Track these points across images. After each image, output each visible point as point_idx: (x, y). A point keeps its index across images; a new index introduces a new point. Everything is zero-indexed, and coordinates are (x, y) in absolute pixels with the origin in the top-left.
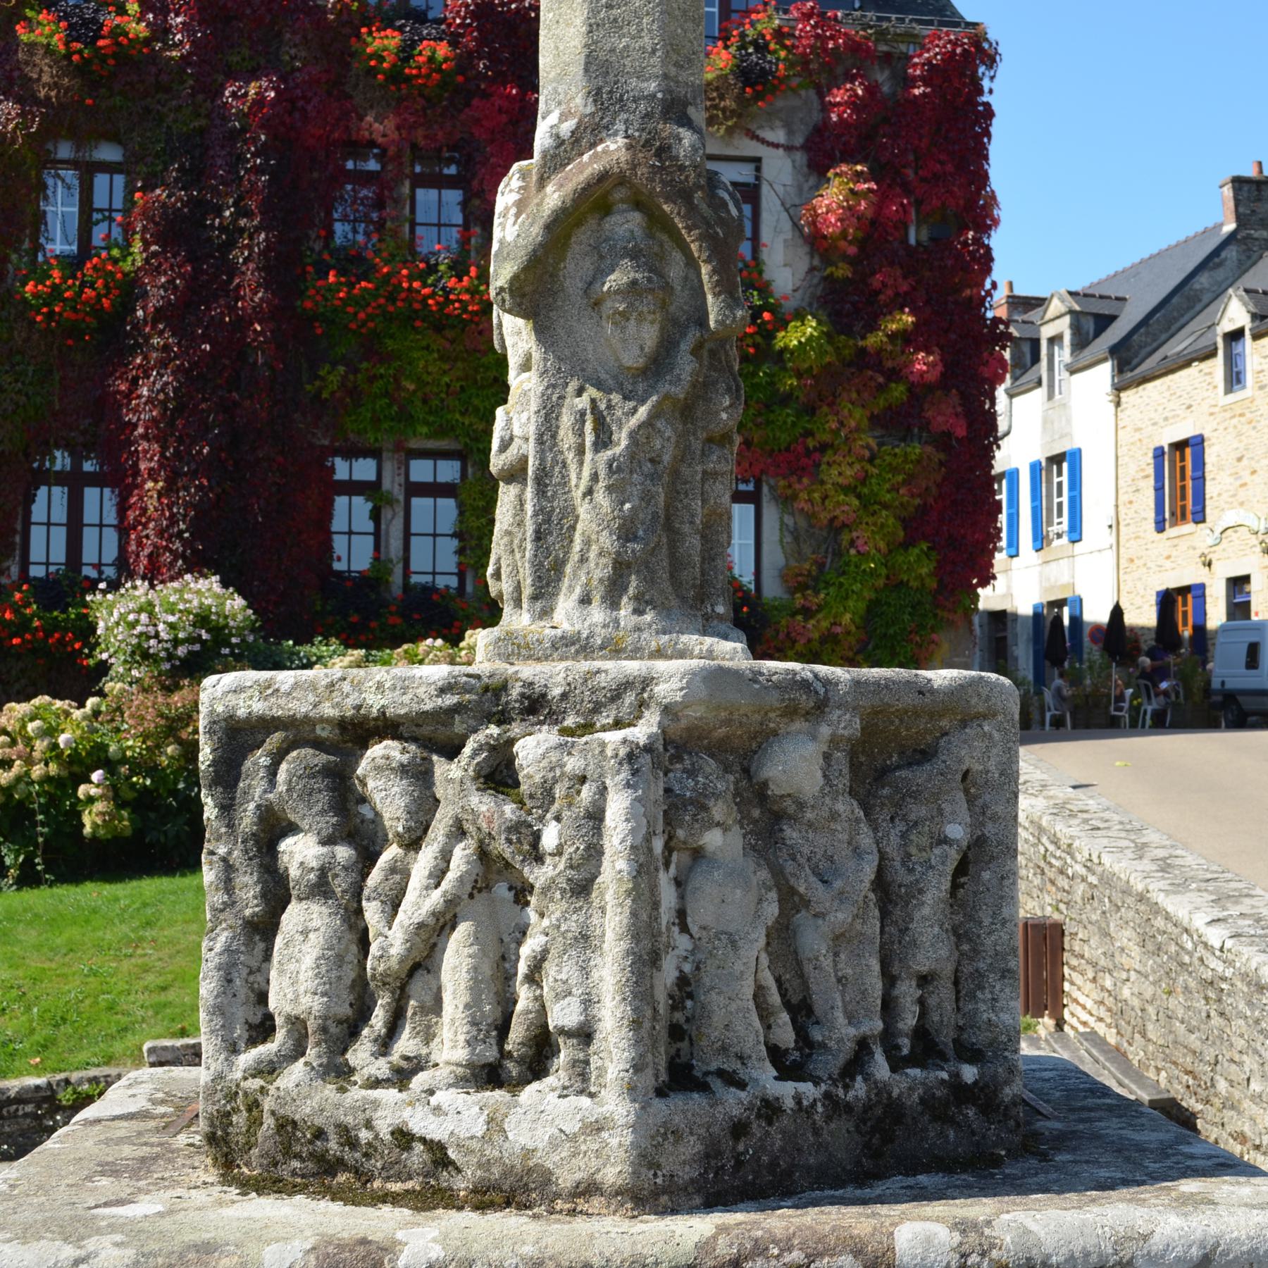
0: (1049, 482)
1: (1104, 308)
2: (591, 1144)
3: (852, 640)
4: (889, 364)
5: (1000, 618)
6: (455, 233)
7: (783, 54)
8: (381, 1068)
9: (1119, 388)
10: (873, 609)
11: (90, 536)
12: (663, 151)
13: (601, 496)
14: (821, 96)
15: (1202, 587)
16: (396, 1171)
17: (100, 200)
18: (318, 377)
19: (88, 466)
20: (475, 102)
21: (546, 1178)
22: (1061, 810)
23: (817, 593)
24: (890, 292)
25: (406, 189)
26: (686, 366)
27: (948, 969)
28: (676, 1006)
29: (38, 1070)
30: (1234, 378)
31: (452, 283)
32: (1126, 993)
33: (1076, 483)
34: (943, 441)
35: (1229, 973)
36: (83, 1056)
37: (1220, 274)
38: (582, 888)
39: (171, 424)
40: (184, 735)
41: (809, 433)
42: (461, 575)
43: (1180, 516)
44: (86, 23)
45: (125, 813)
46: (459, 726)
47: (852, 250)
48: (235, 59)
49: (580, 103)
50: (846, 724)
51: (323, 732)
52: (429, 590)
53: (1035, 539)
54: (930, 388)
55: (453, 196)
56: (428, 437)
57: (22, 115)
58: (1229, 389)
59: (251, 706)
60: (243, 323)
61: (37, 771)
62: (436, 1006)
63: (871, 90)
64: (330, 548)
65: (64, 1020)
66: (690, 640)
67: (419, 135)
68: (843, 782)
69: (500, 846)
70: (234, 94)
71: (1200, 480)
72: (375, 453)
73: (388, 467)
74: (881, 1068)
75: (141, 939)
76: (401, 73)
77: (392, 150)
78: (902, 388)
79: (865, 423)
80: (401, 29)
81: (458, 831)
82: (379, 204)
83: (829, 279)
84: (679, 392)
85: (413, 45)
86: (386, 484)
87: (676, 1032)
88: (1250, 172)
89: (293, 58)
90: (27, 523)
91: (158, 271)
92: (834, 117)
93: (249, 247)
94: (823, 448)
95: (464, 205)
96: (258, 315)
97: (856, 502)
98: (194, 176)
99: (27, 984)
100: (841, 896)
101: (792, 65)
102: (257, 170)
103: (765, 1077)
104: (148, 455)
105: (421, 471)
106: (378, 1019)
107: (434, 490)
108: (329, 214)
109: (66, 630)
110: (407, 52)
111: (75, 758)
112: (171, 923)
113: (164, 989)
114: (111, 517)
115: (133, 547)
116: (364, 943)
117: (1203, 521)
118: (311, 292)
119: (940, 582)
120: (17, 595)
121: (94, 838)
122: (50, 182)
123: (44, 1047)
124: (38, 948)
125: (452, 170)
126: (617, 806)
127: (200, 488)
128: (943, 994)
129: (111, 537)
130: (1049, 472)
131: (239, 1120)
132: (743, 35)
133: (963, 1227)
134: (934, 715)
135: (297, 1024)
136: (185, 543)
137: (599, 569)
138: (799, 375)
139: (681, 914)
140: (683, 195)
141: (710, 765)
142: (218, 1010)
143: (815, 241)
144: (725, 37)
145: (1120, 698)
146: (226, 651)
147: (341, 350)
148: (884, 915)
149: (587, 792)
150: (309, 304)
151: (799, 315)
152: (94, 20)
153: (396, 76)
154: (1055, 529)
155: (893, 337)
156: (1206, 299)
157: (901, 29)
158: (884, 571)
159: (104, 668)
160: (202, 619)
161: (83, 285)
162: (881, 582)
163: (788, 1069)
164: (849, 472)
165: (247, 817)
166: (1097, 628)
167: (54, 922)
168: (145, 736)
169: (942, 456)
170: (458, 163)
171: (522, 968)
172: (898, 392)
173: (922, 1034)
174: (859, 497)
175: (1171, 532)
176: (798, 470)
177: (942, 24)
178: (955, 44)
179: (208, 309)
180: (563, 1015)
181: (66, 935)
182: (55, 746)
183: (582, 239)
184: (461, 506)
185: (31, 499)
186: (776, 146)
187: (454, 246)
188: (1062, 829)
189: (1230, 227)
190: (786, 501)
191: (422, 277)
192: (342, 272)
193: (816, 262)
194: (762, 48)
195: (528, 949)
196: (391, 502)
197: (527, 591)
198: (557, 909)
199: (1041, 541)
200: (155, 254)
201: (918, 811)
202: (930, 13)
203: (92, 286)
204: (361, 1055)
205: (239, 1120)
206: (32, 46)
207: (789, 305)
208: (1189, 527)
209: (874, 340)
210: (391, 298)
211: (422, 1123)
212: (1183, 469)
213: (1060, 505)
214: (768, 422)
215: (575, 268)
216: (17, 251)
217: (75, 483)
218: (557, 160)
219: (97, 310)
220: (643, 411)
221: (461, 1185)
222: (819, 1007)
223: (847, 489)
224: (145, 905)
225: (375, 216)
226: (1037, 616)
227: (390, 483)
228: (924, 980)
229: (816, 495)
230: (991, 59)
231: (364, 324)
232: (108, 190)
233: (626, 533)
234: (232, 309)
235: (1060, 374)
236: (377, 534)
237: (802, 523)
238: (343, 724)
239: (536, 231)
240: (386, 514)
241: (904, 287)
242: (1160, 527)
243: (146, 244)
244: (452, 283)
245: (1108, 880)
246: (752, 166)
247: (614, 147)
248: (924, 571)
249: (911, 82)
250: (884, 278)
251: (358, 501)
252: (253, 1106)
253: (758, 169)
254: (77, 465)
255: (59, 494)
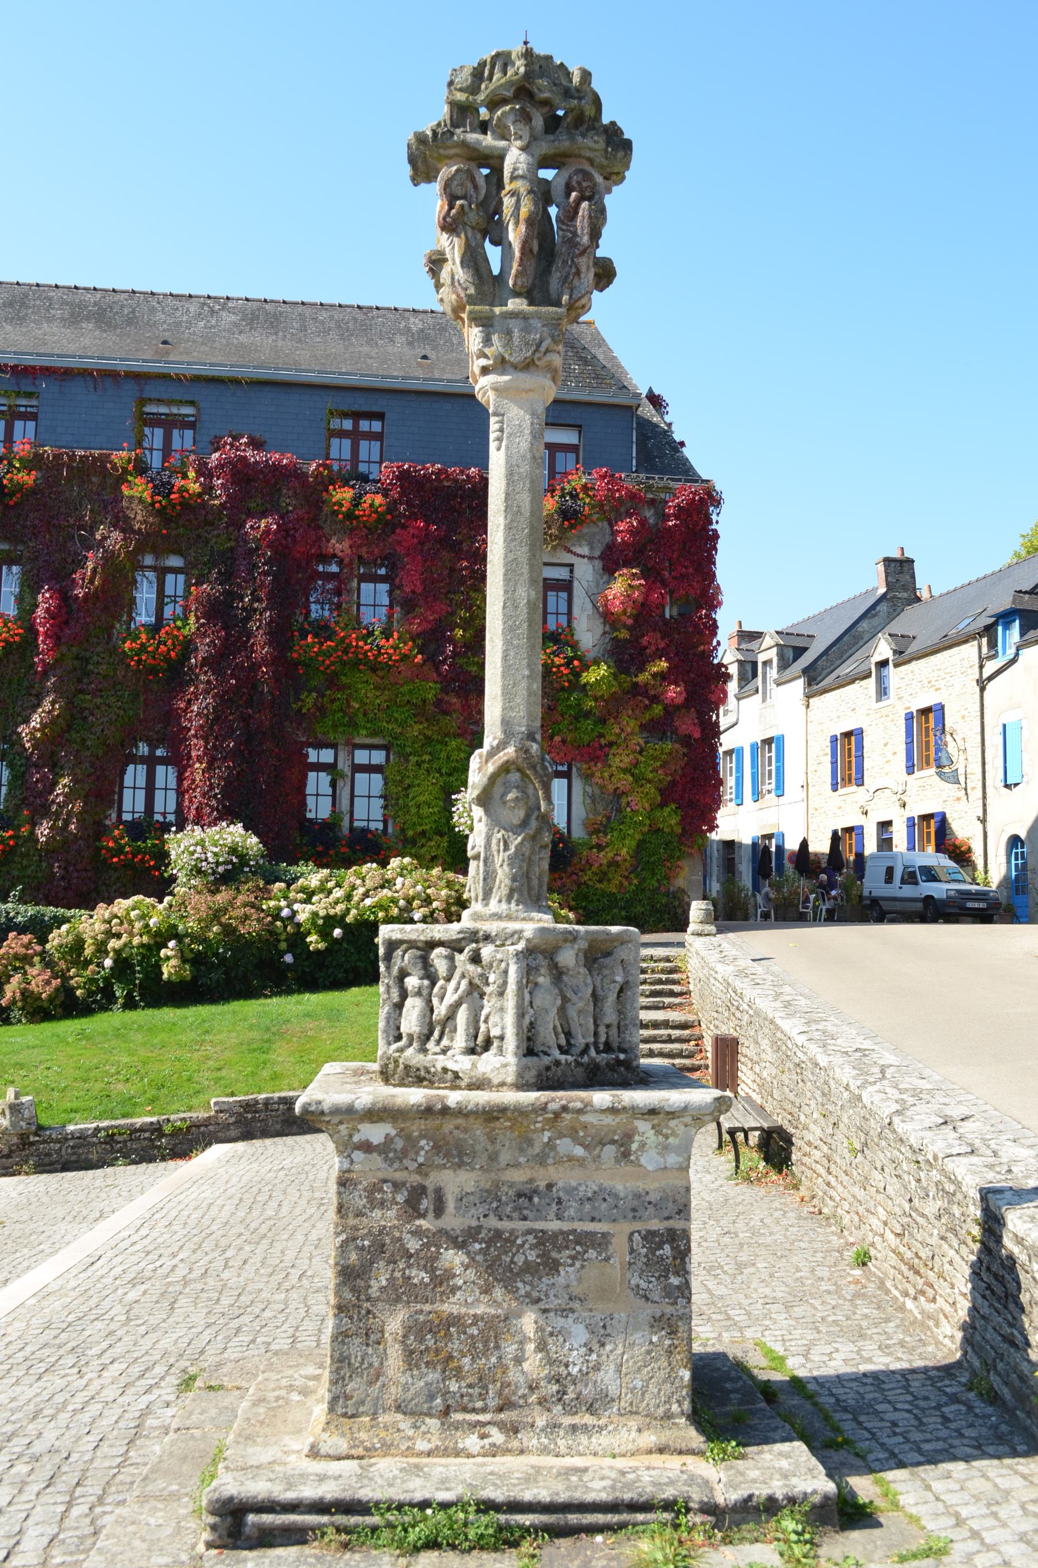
0: (763, 756)
1: (799, 643)
2: (503, 1071)
3: (627, 864)
4: (652, 692)
5: (729, 845)
6: (384, 610)
7: (587, 500)
8: (437, 1049)
9: (808, 696)
10: (641, 845)
11: (159, 795)
12: (527, 751)
13: (505, 867)
14: (611, 526)
15: (862, 827)
16: (442, 1080)
17: (169, 590)
18: (299, 700)
19: (159, 752)
20: (398, 531)
21: (490, 1081)
22: (742, 973)
23: (606, 835)
24: (653, 648)
25: (355, 584)
26: (534, 823)
27: (615, 1023)
28: (529, 1031)
29: (150, 1113)
30: (882, 692)
31: (383, 642)
32: (765, 1074)
33: (780, 757)
34: (686, 741)
35: (804, 1059)
36: (175, 1107)
37: (876, 621)
38: (501, 994)
39: (211, 728)
40: (223, 920)
41: (601, 736)
42: (385, 822)
43: (848, 781)
44: (163, 484)
45: (187, 967)
46: (463, 944)
47: (630, 622)
48: (253, 505)
49: (500, 735)
50: (583, 944)
51: (420, 945)
52: (365, 831)
53: (753, 794)
54: (678, 707)
55: (383, 588)
56: (366, 736)
57: (124, 539)
58: (879, 699)
59: (396, 936)
60: (255, 667)
61: (136, 941)
62: (455, 1030)
63: (642, 522)
64: (305, 804)
65: (163, 1086)
66: (536, 915)
67: (363, 551)
68: (582, 963)
69: (477, 981)
70: (252, 527)
71: (861, 758)
72: (333, 746)
73: (342, 755)
74: (593, 1052)
75: (204, 1041)
76: (353, 513)
77: (346, 561)
78: (660, 707)
79: (637, 729)
80: (353, 487)
81: (463, 976)
82: (338, 592)
83: (615, 639)
84: (531, 832)
85: (360, 496)
86: (340, 765)
87: (529, 1039)
88: (896, 554)
89: (288, 505)
90: (122, 787)
91: (205, 635)
92: (619, 539)
93: (260, 621)
94: (611, 744)
95: (390, 593)
96: (264, 662)
97: (631, 779)
98: (226, 577)
99: (140, 1065)
100: (581, 998)
101: (593, 507)
102: (265, 574)
103: (556, 1054)
104: (197, 748)
105: (361, 757)
106: (436, 1034)
107: (370, 769)
108: (307, 599)
109: (145, 853)
110: (356, 501)
111: (158, 933)
112: (221, 1032)
113: (219, 1069)
114: (173, 783)
115: (187, 803)
116: (432, 1011)
117: (862, 784)
118: (297, 648)
119: (683, 829)
120: (116, 832)
121: (169, 982)
122: (139, 578)
123: (153, 1101)
124: (144, 1044)
125: (382, 571)
126: (513, 969)
127: (228, 767)
128: (614, 1031)
129: (172, 796)
130: (763, 749)
131: (391, 1066)
132: (563, 489)
133: (614, 1096)
134: (612, 941)
135: (411, 1037)
136: (218, 801)
137: (505, 891)
138: (596, 699)
139: (531, 1003)
140: (533, 767)
141: (540, 957)
142: (385, 1031)
143: (607, 616)
144: (551, 490)
145: (807, 900)
146: (247, 869)
147: (314, 683)
148: (595, 1005)
149: (503, 965)
150: (295, 655)
151: (596, 662)
152: (169, 483)
153: (350, 516)
154: (766, 787)
155: (654, 675)
156: (866, 638)
157: (661, 484)
158: (648, 822)
159: (173, 879)
160: (233, 850)
161: (160, 643)
162: (646, 829)
163: (563, 1050)
164: (626, 760)
165: (395, 971)
166: (793, 853)
167: (151, 1030)
168: (200, 921)
169: (685, 750)
170: (386, 567)
171: (482, 1018)
172: (658, 710)
173: (607, 1044)
174: (632, 775)
175: (841, 791)
176: (596, 759)
177: (687, 481)
178: (695, 494)
179: (235, 658)
180: (495, 1032)
181: (160, 1038)
182: (147, 925)
183: (500, 780)
184: (385, 780)
185: (123, 772)
186: (583, 557)
187: (384, 618)
188: (738, 984)
189: (882, 590)
190: (587, 777)
191: (364, 638)
192: (316, 635)
193: (607, 629)
194: (574, 496)
195: (484, 1013)
196: (342, 776)
197: (480, 897)
198: (493, 1000)
199: (757, 795)
200: (203, 625)
201: (606, 972)
202: (680, 474)
203: (165, 644)
204: (431, 1045)
205: (391, 1066)
206: (131, 497)
207: (590, 656)
208: (854, 788)
209: (643, 678)
210: (346, 651)
211: (451, 1066)
212: (850, 750)
213: (770, 771)
214: (576, 729)
215: (498, 790)
216: (119, 621)
217: (152, 763)
218: (492, 754)
219: (167, 659)
220: (519, 839)
221: (463, 1084)
222: (573, 1033)
223: (625, 771)
224: (204, 1021)
225: (336, 600)
226: (754, 845)
227: (343, 765)
228: (608, 1026)
229: (606, 774)
230: (717, 502)
231: (328, 667)
232: (175, 584)
233: (514, 879)
234: (249, 658)
235: (771, 686)
236: (334, 796)
237: (597, 791)
238: (426, 942)
239: (485, 780)
240: (340, 784)
241: (662, 645)
242: (835, 788)
243: (198, 618)
244: (383, 642)
245: (758, 1013)
246: (568, 569)
247: (510, 751)
248: (673, 822)
249: (666, 517)
250: (650, 640)
251: (323, 775)
252: (396, 1061)
253: (571, 571)
254: (152, 752)
255: (142, 770)
